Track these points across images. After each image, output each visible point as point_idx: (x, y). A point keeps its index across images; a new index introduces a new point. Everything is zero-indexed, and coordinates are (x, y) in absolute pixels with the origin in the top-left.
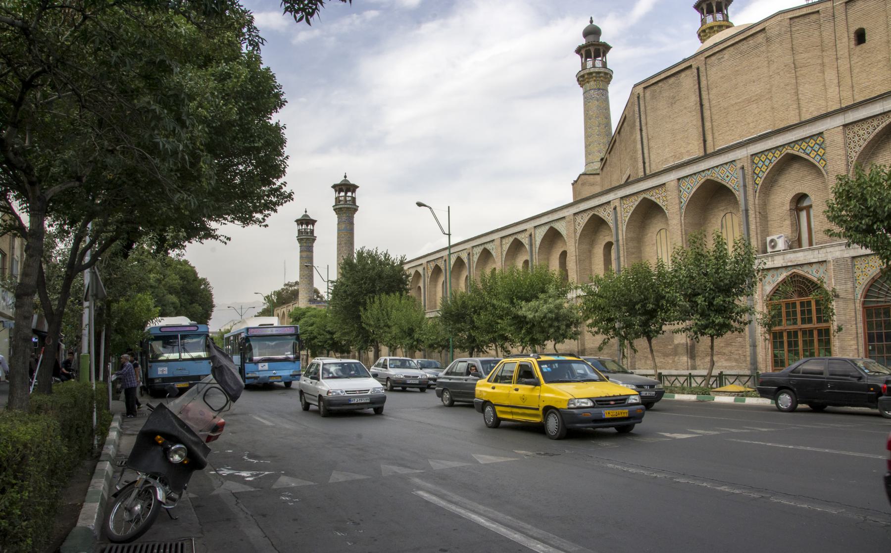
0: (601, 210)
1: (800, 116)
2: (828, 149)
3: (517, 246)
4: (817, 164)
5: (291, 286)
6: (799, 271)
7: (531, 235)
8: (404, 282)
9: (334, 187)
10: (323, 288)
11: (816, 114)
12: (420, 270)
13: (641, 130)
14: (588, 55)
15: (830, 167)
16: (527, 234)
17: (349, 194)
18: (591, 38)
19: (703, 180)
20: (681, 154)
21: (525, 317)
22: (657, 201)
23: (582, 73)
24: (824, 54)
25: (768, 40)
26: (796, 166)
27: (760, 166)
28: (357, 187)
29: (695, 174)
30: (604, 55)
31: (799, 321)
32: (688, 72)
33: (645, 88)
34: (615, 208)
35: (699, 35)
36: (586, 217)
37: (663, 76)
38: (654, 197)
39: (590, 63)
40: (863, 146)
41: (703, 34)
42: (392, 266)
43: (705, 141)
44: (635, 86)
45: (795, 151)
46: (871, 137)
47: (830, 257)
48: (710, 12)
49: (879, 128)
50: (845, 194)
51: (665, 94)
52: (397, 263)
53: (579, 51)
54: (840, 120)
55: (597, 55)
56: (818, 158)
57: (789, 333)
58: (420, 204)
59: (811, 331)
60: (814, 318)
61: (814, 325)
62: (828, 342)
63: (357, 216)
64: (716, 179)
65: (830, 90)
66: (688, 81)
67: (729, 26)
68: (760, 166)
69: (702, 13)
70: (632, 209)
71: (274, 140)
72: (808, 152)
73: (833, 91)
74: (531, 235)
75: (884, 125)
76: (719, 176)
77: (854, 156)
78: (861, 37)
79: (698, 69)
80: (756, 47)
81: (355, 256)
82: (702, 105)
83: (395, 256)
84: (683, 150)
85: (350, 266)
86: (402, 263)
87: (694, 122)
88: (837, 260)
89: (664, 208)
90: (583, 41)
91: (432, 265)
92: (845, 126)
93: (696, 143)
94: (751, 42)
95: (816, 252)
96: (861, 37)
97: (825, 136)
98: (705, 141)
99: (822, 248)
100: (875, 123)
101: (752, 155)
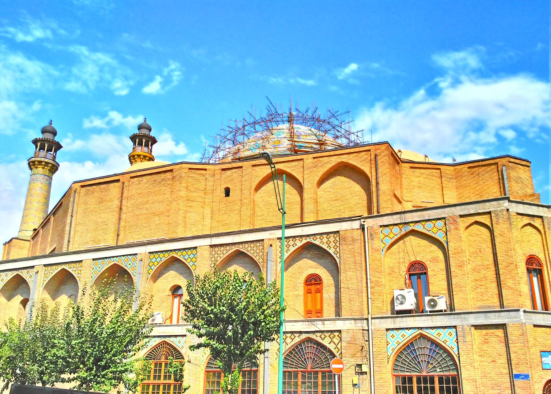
0: (25, 271)
1: (317, 213)
2: (198, 259)
4: (190, 267)
6: (167, 340)
13: (72, 216)
18: (48, 136)
20: (100, 240)
22: (73, 273)
23: (33, 159)
24: (206, 196)
25: (173, 178)
26: (177, 265)
27: (153, 261)
30: (56, 151)
31: (152, 377)
32: (116, 184)
33: (82, 186)
34: (37, 273)
35: (130, 158)
37: (154, 171)
39: (43, 153)
43: (118, 235)
44: (75, 182)
45: (178, 255)
46: (225, 256)
48: (140, 144)
49: (230, 252)
51: (96, 195)
54: (278, 233)
55: (49, 150)
56: (191, 263)
57: (154, 386)
59: (169, 385)
66: (115, 189)
67: (151, 159)
68: (153, 261)
69: (135, 144)
70: (52, 276)
72: (186, 258)
75: (232, 251)
76: (122, 262)
78: (227, 192)
79: (123, 183)
80: (163, 180)
84: (100, 238)
87: (113, 220)
89: (78, 279)
92: (212, 246)
93: (112, 235)
94: (163, 176)
96: (227, 192)
97: (198, 249)
98: (118, 235)
100: (228, 248)
101: (149, 253)
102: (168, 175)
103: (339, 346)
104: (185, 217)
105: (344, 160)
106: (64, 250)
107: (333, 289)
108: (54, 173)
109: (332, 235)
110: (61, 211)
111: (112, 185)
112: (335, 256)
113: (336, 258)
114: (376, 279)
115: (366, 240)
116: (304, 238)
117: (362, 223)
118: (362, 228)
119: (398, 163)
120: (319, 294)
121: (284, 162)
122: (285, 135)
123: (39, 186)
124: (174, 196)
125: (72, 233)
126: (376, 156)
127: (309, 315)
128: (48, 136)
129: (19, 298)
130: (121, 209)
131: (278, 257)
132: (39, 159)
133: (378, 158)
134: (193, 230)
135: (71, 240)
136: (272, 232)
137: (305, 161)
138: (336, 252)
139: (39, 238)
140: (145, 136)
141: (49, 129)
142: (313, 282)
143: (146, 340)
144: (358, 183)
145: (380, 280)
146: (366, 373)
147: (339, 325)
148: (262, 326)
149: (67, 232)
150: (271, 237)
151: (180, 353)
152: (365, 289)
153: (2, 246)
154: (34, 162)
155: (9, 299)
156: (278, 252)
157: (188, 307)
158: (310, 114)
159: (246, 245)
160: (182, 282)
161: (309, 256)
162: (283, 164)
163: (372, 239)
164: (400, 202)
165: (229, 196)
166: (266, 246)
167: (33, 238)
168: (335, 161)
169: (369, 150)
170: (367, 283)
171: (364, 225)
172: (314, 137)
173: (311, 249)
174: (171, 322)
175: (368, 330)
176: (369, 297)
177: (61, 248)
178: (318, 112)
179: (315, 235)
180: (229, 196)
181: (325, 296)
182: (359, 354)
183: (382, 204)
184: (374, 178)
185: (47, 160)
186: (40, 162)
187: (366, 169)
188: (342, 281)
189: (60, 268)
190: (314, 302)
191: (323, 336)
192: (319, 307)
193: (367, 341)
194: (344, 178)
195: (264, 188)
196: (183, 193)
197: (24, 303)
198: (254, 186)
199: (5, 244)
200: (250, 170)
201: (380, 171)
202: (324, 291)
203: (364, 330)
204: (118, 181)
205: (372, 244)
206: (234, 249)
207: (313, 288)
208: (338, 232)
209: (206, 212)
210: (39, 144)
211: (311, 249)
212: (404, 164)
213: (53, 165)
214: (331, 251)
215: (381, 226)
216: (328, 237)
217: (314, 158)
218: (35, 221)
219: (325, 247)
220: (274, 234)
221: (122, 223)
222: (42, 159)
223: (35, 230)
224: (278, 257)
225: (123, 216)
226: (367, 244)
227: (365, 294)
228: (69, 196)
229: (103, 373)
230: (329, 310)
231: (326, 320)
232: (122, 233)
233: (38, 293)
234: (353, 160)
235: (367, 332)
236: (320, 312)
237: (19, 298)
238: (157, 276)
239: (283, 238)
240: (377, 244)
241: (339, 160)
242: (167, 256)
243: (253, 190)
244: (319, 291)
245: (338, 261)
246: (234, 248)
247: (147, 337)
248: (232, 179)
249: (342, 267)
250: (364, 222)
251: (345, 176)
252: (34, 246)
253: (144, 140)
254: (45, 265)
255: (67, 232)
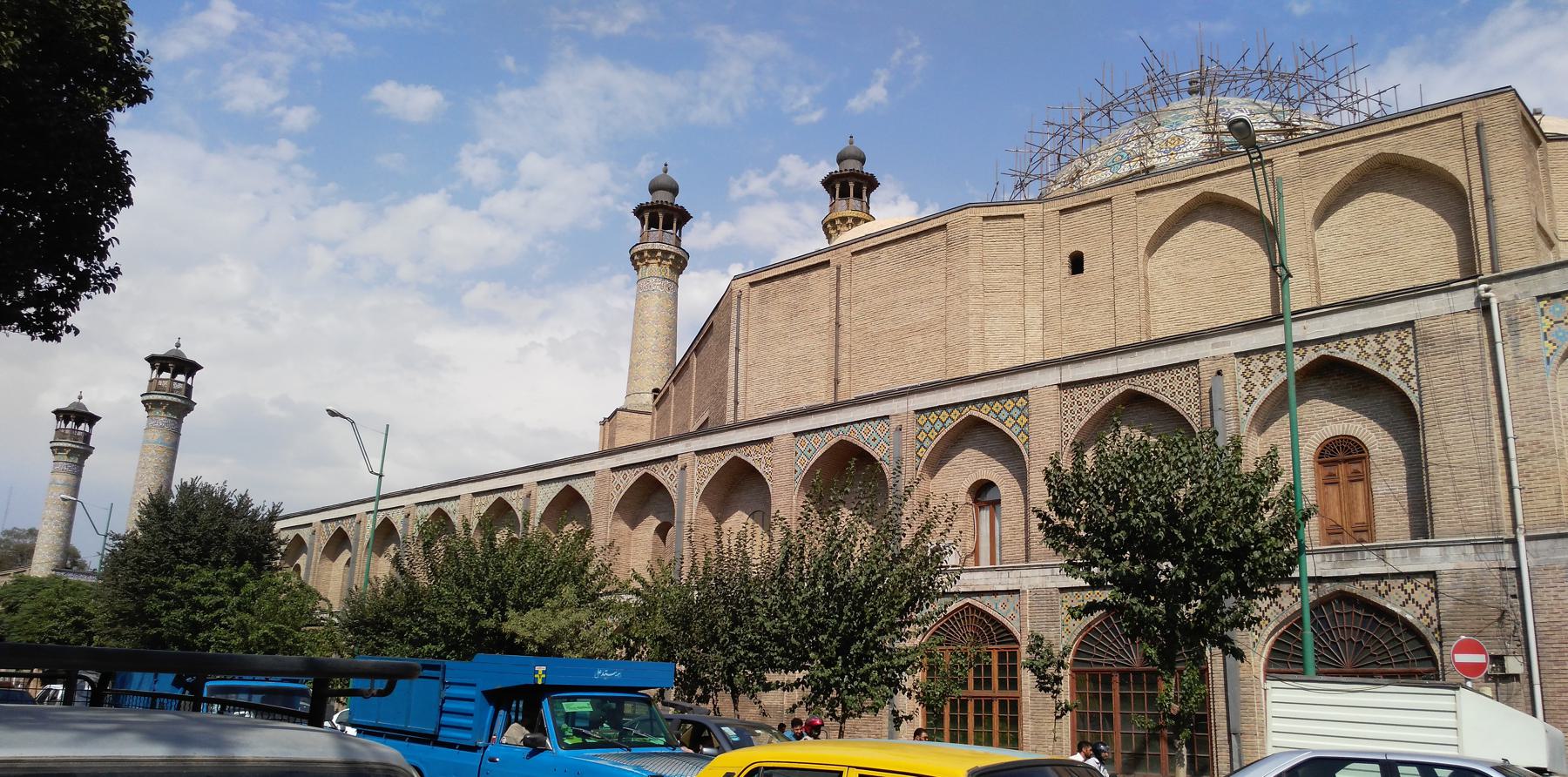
0: (660, 467)
2: (1032, 417)
3: (501, 511)
5: (18, 536)
7: (529, 496)
8: (272, 553)
9: (152, 360)
10: (92, 551)
11: (1008, 365)
12: (305, 534)
13: (737, 349)
14: (653, 223)
15: (1033, 445)
16: (522, 493)
17: (180, 377)
19: (835, 441)
20: (798, 397)
21: (514, 635)
23: (639, 248)
26: (980, 435)
28: (199, 367)
29: (823, 429)
30: (679, 227)
33: (752, 284)
34: (684, 468)
35: (825, 227)
36: (633, 476)
38: (752, 457)
39: (656, 233)
40: (1086, 420)
41: (830, 226)
42: (253, 520)
43: (837, 382)
44: (736, 278)
45: (982, 413)
47: (1025, 586)
48: (844, 194)
49: (1109, 397)
50: (1063, 491)
52: (264, 514)
53: (639, 212)
54: (1053, 376)
55: (667, 226)
58: (332, 413)
60: (995, 682)
61: (995, 691)
62: (1015, 722)
63: (188, 419)
64: (856, 442)
65: (1031, 333)
66: (820, 282)
69: (833, 196)
71: (110, 182)
73: (1035, 335)
74: (529, 496)
75: (1116, 393)
76: (859, 437)
77: (1072, 435)
78: (1077, 263)
79: (838, 268)
80: (929, 251)
81: (175, 492)
82: (838, 325)
83: (261, 501)
85: (159, 511)
86: (274, 516)
87: (824, 350)
88: (1035, 591)
90: (647, 198)
91: (333, 528)
94: (923, 240)
95: (1005, 574)
96: (1077, 263)
97: (1031, 396)
98: (837, 382)
99: (1014, 568)
102: (938, 237)
103: (1432, 611)
104: (982, 330)
105: (1386, 150)
106: (729, 420)
107: (1401, 471)
108: (680, 272)
109: (1392, 334)
110: (711, 342)
111: (814, 274)
112: (1403, 386)
113: (1409, 392)
114: (1533, 436)
115: (1498, 338)
116: (1309, 348)
117: (1484, 294)
118: (1484, 307)
119: (1538, 143)
120: (1360, 485)
121: (1219, 174)
122: (1192, 122)
123: (655, 302)
124: (953, 284)
125: (741, 384)
126: (1479, 127)
127: (1334, 538)
128: (663, 197)
129: (652, 523)
130: (838, 325)
131: (1240, 401)
132: (650, 246)
133: (1488, 134)
134: (1002, 357)
135: (740, 399)
136: (1220, 339)
137: (1278, 164)
138: (1407, 377)
139: (671, 404)
140: (855, 175)
141: (662, 181)
142: (1341, 455)
143: (943, 600)
144: (1428, 205)
145: (1546, 438)
146: (1517, 677)
147: (1429, 559)
148: (1255, 561)
149: (731, 384)
150: (1218, 352)
151: (1008, 631)
152: (1500, 466)
153: (598, 428)
154: (641, 253)
155: (633, 524)
156: (1240, 388)
157: (1049, 521)
158: (1251, 64)
159: (1152, 378)
160: (993, 470)
161: (1323, 391)
162: (1218, 180)
163: (1516, 333)
164: (1551, 245)
165: (1081, 271)
166: (1205, 376)
167: (657, 406)
168: (1359, 155)
169: (1459, 115)
170: (1506, 449)
171: (1488, 299)
172: (1268, 118)
173: (1332, 376)
174: (977, 563)
175: (1518, 570)
176: (1516, 483)
177: (723, 417)
178: (1274, 59)
179: (1341, 337)
180: (1081, 271)
181: (1379, 488)
182: (1494, 631)
183: (1505, 250)
184: (1477, 183)
185: (665, 247)
186: (653, 252)
187: (1454, 164)
188: (1430, 445)
189: (729, 455)
190: (1348, 505)
191: (1383, 587)
192: (1361, 516)
193: (1514, 596)
194: (1387, 195)
195: (1168, 244)
196: (974, 277)
197: (662, 531)
198: (1144, 243)
199: (603, 424)
200: (1131, 201)
201: (1494, 166)
202: (1375, 478)
203: (1503, 569)
204: (826, 264)
205: (1516, 347)
206: (1122, 390)
207: (1342, 471)
208: (1411, 324)
209: (1028, 315)
210: (646, 216)
211: (1332, 376)
212: (1550, 145)
213: (677, 256)
214: (1394, 374)
215: (1540, 298)
216: (1382, 338)
217: (1301, 154)
218: (655, 375)
219: (1373, 365)
220: (1224, 344)
221: (844, 356)
222: (657, 246)
223: (656, 390)
224: (1240, 401)
225: (845, 340)
226: (1499, 347)
227: (1501, 478)
228: (729, 305)
229: (861, 671)
230: (1392, 519)
231: (1388, 547)
232: (844, 377)
233: (691, 510)
234: (1412, 147)
235: (1513, 574)
236: (1366, 529)
237: (652, 523)
238: (936, 463)
239: (1289, 347)
240: (1531, 344)
241: (1373, 152)
242: (957, 417)
243: (1142, 252)
244: (1363, 477)
245: (1414, 398)
246: (1122, 387)
247: (945, 594)
248: (1084, 232)
249: (1428, 413)
250: (1487, 290)
251: (1389, 191)
252: (663, 419)
253: (851, 185)
254: (698, 453)
255: (731, 384)
